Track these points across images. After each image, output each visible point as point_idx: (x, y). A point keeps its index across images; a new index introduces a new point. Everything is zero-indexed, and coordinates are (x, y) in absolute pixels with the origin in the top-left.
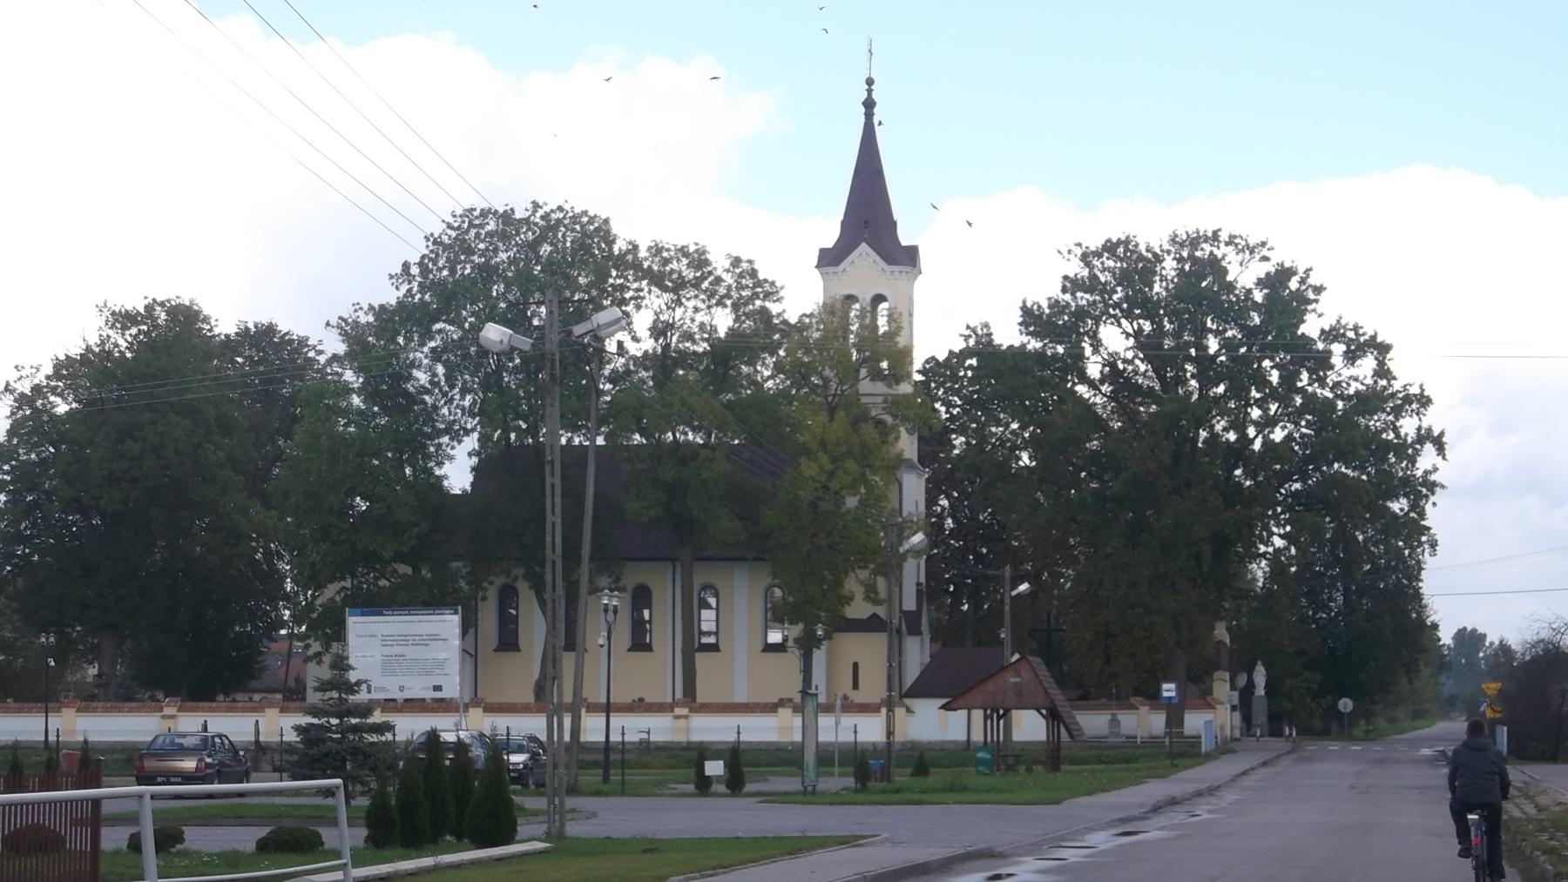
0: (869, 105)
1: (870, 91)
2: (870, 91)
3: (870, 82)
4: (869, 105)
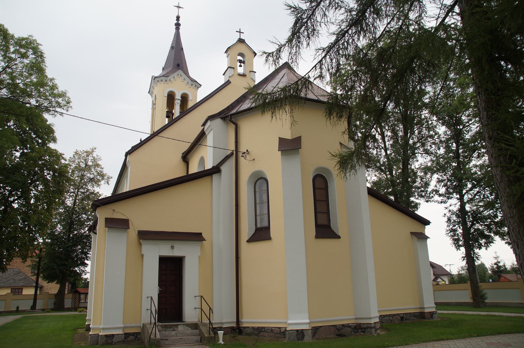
0: (178, 25)
3: (178, 18)
4: (178, 25)
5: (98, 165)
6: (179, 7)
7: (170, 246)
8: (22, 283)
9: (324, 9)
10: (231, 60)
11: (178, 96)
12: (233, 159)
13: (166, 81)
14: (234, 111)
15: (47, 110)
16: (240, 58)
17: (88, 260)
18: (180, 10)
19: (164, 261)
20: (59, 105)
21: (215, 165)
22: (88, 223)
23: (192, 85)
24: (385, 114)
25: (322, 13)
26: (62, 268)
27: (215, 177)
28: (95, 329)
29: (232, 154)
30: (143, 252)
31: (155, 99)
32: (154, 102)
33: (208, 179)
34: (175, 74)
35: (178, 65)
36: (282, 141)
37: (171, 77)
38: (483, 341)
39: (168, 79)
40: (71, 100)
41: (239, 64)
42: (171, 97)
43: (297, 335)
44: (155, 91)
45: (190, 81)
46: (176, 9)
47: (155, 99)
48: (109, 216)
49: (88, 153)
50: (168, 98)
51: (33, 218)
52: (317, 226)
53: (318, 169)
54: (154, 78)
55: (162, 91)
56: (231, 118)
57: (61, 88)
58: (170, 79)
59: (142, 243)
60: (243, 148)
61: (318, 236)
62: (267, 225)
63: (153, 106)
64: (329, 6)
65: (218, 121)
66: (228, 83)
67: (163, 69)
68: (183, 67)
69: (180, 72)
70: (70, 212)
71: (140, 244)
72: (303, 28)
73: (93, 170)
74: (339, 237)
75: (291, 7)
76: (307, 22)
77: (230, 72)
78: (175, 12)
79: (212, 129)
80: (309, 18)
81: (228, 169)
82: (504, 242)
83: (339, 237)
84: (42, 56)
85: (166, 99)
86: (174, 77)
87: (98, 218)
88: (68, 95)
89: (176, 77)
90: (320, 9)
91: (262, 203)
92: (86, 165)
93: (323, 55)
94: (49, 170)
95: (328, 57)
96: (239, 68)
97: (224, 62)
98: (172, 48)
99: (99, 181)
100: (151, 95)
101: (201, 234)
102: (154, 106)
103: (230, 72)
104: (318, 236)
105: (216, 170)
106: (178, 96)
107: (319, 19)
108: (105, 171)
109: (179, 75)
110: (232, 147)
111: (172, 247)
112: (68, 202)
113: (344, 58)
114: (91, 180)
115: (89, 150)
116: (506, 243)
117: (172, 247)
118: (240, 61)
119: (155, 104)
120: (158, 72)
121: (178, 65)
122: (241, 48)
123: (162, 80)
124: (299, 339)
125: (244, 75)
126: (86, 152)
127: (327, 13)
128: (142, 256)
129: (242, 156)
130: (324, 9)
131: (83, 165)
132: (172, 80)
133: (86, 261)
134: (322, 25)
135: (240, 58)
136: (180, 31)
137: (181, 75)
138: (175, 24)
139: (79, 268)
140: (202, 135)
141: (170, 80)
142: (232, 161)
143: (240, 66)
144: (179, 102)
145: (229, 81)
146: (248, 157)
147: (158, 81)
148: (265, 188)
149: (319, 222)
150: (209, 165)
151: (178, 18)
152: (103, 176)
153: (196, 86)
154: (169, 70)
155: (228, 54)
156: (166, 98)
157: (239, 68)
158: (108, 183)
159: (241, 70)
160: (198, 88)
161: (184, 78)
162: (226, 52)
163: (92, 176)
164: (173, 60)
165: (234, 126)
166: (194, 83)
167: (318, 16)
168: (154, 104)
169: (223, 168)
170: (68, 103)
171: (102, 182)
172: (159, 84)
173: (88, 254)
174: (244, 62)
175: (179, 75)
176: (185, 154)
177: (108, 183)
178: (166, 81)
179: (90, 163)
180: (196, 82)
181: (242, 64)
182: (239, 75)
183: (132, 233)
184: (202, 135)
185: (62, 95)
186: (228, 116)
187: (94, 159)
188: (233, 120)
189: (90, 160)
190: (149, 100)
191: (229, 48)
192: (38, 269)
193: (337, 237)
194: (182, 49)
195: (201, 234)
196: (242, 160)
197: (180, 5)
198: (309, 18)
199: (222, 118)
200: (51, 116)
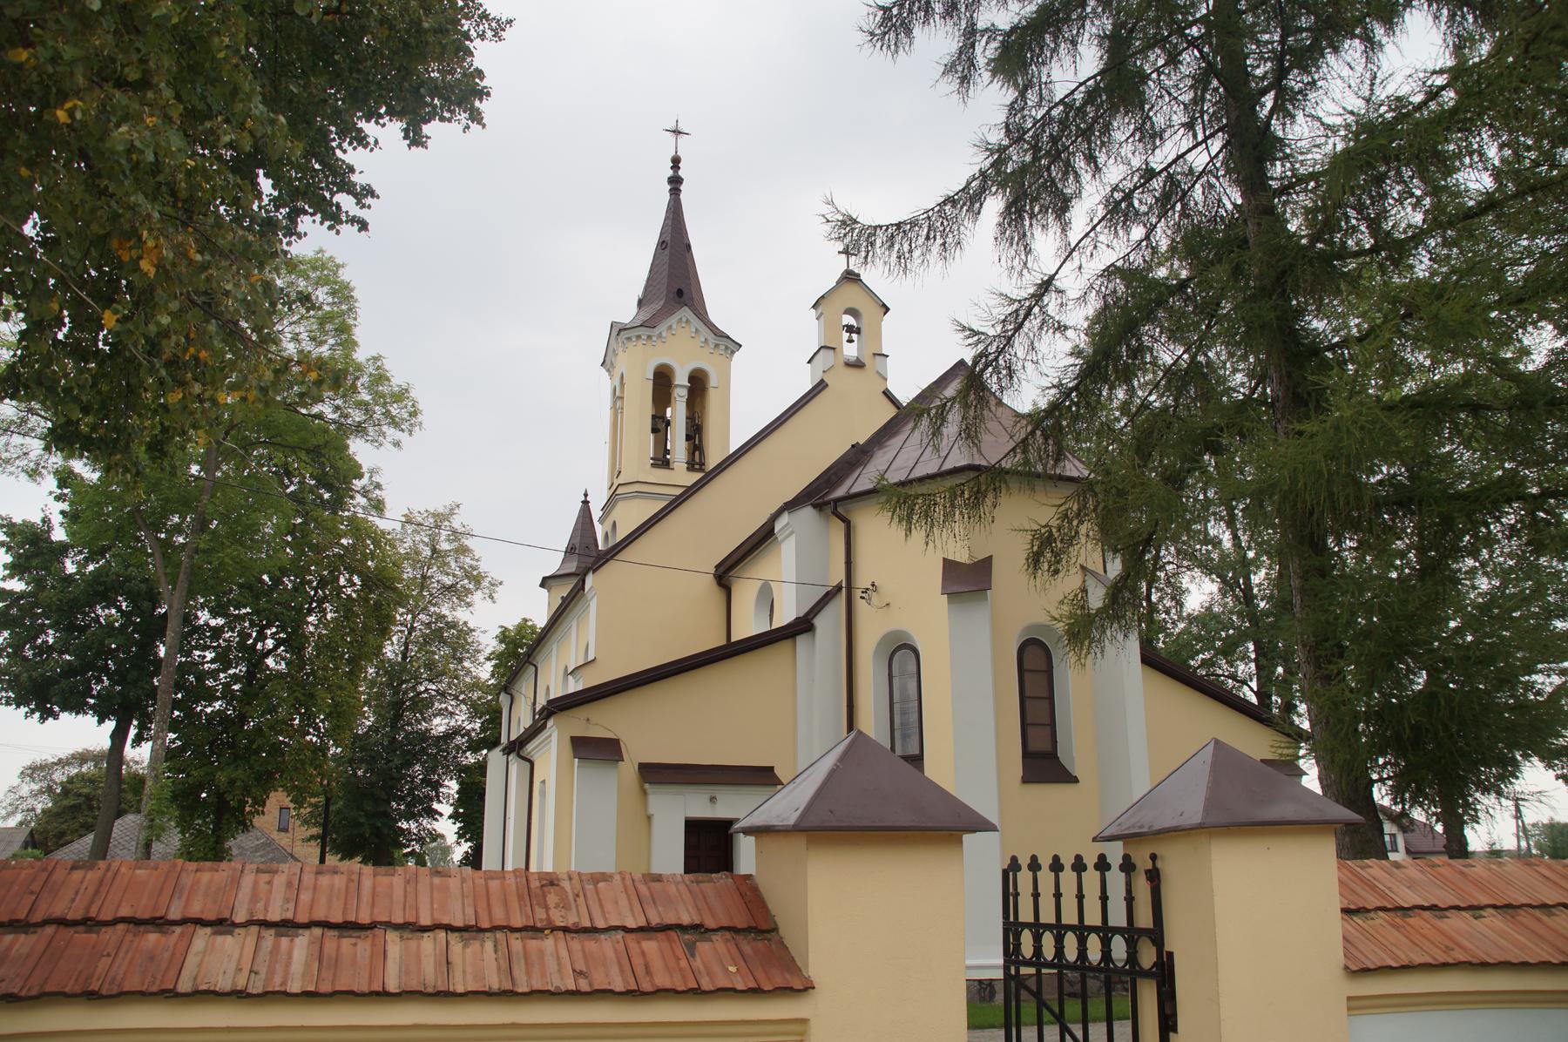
0: (675, 182)
3: (676, 162)
4: (675, 182)
5: (464, 550)
6: (677, 132)
7: (707, 797)
8: (261, 856)
9: (1031, 335)
10: (828, 326)
11: (681, 379)
12: (840, 602)
13: (649, 337)
14: (840, 492)
15: (359, 429)
16: (848, 320)
17: (440, 802)
18: (682, 139)
19: (694, 828)
20: (395, 423)
21: (801, 615)
22: (444, 706)
23: (717, 346)
25: (1027, 343)
26: (379, 824)
27: (802, 640)
29: (838, 588)
30: (651, 811)
31: (622, 384)
32: (618, 393)
33: (784, 646)
34: (673, 320)
35: (680, 293)
36: (950, 567)
37: (662, 328)
39: (656, 331)
40: (420, 407)
41: (846, 336)
42: (662, 380)
43: (979, 992)
44: (622, 363)
45: (712, 339)
47: (622, 384)
48: (580, 733)
49: (440, 519)
50: (654, 384)
51: (323, 699)
52: (1027, 754)
53: (1029, 628)
54: (618, 330)
55: (640, 364)
56: (836, 508)
57: (398, 380)
59: (649, 791)
60: (862, 581)
61: (1027, 779)
62: (917, 752)
63: (615, 403)
64: (1041, 328)
65: (807, 514)
66: (821, 386)
67: (640, 303)
68: (692, 299)
69: (686, 313)
70: (396, 674)
71: (644, 793)
72: (990, 369)
73: (453, 565)
74: (1075, 780)
75: (964, 329)
76: (996, 359)
77: (825, 359)
79: (792, 532)
80: (1000, 352)
81: (829, 624)
82: (1551, 774)
83: (1075, 780)
84: (348, 298)
85: (649, 387)
86: (670, 327)
88: (413, 394)
89: (674, 326)
90: (1022, 335)
91: (905, 700)
92: (434, 550)
93: (1029, 428)
94: (352, 571)
95: (1038, 433)
96: (846, 346)
97: (809, 332)
98: (662, 245)
99: (468, 592)
100: (608, 371)
101: (771, 769)
102: (619, 403)
103: (825, 359)
104: (1027, 779)
105: (803, 626)
106: (681, 379)
107: (1021, 354)
108: (483, 567)
110: (838, 575)
111: (713, 799)
112: (390, 648)
114: (449, 589)
115: (441, 510)
116: (1557, 777)
117: (713, 799)
118: (850, 329)
119: (622, 398)
120: (627, 313)
121: (680, 293)
122: (851, 296)
123: (639, 337)
124: (983, 999)
125: (857, 365)
126: (434, 515)
127: (1036, 344)
128: (649, 818)
129: (862, 598)
130: (1031, 335)
131: (427, 552)
132: (664, 334)
133: (435, 806)
134: (1029, 365)
135: (848, 320)
136: (682, 196)
137: (687, 321)
140: (763, 538)
141: (660, 335)
142: (839, 605)
143: (850, 341)
144: (684, 392)
145: (822, 381)
146: (875, 597)
147: (629, 339)
148: (912, 668)
149: (1032, 747)
150: (786, 614)
151: (676, 162)
152: (477, 580)
153: (727, 348)
154: (657, 306)
155: (820, 311)
156: (650, 385)
157: (846, 346)
158: (491, 597)
159: (850, 351)
160: (733, 352)
162: (815, 306)
163: (448, 581)
164: (665, 280)
165: (842, 525)
166: (724, 342)
167: (1019, 347)
168: (617, 398)
169: (819, 622)
170: (414, 414)
171: (477, 597)
172: (630, 345)
173: (442, 786)
174: (858, 331)
176: (722, 569)
177: (491, 597)
178: (649, 337)
179: (444, 546)
180: (728, 337)
181: (855, 336)
182: (848, 364)
183: (628, 769)
184: (763, 538)
185: (401, 396)
186: (828, 503)
187: (455, 535)
188: (840, 510)
189: (443, 538)
190: (603, 384)
191: (823, 297)
192: (325, 826)
193: (1074, 780)
194: (688, 247)
195: (771, 769)
196: (861, 606)
197: (682, 127)
198: (1000, 352)
199: (815, 506)
200: (368, 444)
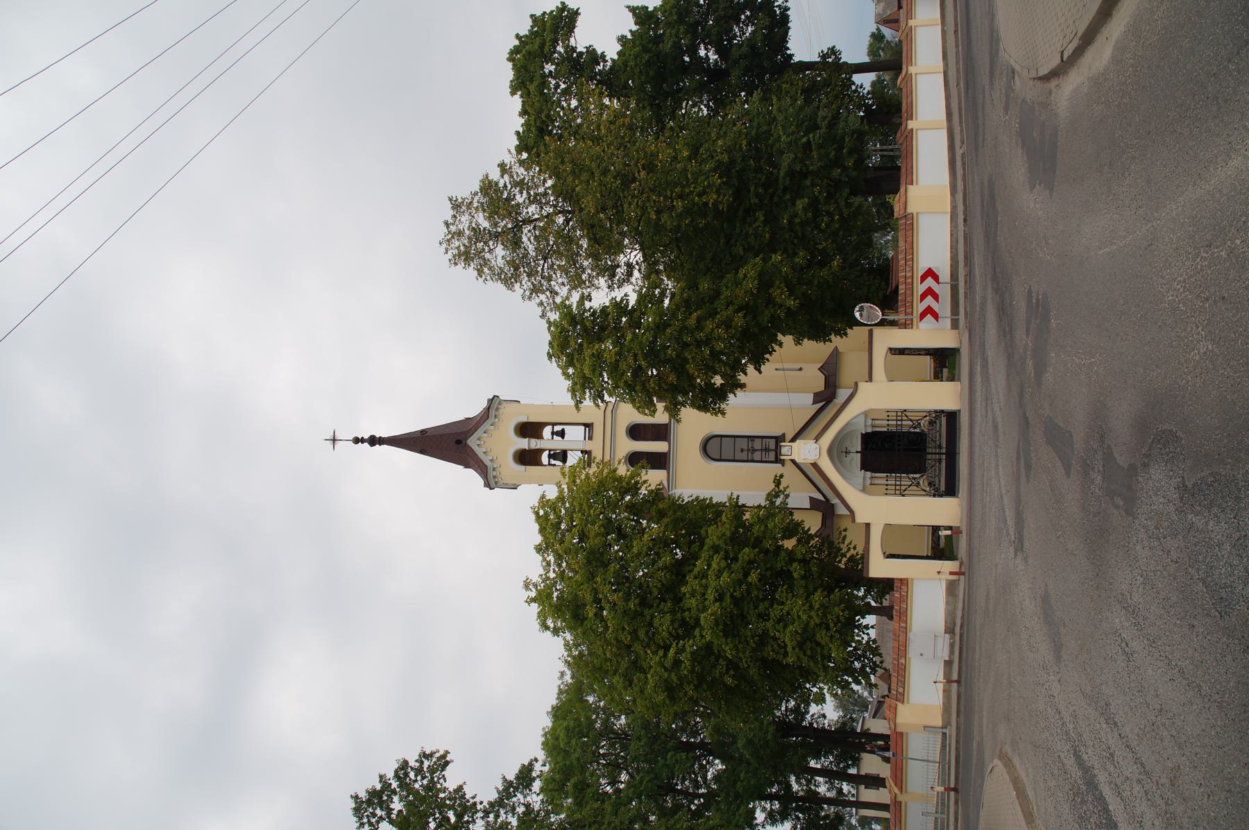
0: (373, 441)
1: (362, 440)
2: (362, 440)
3: (357, 440)
4: (373, 441)
24: (711, 333)
28: (928, 552)
34: (479, 452)
38: (907, 136)
46: (338, 444)
58: (491, 460)
69: (472, 442)
78: (346, 447)
87: (896, 785)
109: (478, 442)
113: (515, 818)
120: (472, 475)
121: (459, 442)
136: (384, 436)
138: (371, 446)
139: (671, 371)
147: (497, 409)
151: (357, 440)
161: (485, 432)
172: (501, 411)
175: (478, 442)
194: (423, 432)
